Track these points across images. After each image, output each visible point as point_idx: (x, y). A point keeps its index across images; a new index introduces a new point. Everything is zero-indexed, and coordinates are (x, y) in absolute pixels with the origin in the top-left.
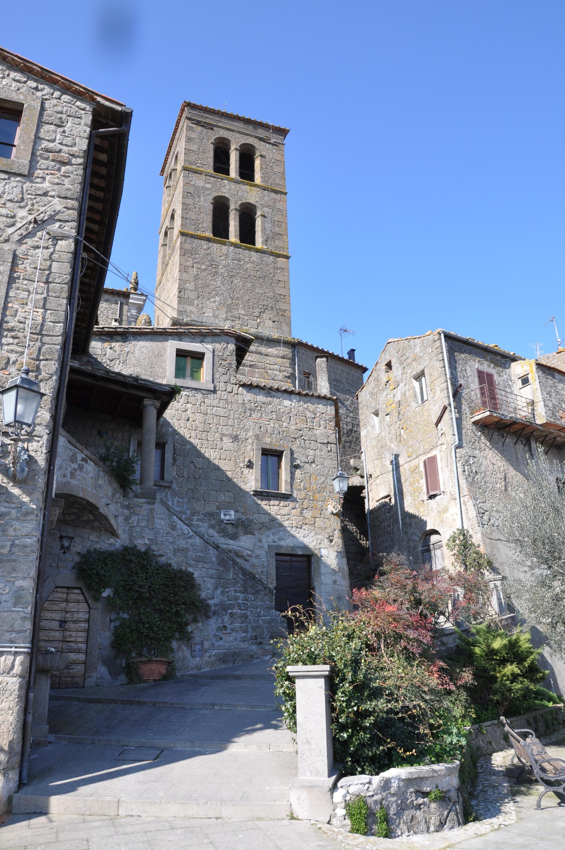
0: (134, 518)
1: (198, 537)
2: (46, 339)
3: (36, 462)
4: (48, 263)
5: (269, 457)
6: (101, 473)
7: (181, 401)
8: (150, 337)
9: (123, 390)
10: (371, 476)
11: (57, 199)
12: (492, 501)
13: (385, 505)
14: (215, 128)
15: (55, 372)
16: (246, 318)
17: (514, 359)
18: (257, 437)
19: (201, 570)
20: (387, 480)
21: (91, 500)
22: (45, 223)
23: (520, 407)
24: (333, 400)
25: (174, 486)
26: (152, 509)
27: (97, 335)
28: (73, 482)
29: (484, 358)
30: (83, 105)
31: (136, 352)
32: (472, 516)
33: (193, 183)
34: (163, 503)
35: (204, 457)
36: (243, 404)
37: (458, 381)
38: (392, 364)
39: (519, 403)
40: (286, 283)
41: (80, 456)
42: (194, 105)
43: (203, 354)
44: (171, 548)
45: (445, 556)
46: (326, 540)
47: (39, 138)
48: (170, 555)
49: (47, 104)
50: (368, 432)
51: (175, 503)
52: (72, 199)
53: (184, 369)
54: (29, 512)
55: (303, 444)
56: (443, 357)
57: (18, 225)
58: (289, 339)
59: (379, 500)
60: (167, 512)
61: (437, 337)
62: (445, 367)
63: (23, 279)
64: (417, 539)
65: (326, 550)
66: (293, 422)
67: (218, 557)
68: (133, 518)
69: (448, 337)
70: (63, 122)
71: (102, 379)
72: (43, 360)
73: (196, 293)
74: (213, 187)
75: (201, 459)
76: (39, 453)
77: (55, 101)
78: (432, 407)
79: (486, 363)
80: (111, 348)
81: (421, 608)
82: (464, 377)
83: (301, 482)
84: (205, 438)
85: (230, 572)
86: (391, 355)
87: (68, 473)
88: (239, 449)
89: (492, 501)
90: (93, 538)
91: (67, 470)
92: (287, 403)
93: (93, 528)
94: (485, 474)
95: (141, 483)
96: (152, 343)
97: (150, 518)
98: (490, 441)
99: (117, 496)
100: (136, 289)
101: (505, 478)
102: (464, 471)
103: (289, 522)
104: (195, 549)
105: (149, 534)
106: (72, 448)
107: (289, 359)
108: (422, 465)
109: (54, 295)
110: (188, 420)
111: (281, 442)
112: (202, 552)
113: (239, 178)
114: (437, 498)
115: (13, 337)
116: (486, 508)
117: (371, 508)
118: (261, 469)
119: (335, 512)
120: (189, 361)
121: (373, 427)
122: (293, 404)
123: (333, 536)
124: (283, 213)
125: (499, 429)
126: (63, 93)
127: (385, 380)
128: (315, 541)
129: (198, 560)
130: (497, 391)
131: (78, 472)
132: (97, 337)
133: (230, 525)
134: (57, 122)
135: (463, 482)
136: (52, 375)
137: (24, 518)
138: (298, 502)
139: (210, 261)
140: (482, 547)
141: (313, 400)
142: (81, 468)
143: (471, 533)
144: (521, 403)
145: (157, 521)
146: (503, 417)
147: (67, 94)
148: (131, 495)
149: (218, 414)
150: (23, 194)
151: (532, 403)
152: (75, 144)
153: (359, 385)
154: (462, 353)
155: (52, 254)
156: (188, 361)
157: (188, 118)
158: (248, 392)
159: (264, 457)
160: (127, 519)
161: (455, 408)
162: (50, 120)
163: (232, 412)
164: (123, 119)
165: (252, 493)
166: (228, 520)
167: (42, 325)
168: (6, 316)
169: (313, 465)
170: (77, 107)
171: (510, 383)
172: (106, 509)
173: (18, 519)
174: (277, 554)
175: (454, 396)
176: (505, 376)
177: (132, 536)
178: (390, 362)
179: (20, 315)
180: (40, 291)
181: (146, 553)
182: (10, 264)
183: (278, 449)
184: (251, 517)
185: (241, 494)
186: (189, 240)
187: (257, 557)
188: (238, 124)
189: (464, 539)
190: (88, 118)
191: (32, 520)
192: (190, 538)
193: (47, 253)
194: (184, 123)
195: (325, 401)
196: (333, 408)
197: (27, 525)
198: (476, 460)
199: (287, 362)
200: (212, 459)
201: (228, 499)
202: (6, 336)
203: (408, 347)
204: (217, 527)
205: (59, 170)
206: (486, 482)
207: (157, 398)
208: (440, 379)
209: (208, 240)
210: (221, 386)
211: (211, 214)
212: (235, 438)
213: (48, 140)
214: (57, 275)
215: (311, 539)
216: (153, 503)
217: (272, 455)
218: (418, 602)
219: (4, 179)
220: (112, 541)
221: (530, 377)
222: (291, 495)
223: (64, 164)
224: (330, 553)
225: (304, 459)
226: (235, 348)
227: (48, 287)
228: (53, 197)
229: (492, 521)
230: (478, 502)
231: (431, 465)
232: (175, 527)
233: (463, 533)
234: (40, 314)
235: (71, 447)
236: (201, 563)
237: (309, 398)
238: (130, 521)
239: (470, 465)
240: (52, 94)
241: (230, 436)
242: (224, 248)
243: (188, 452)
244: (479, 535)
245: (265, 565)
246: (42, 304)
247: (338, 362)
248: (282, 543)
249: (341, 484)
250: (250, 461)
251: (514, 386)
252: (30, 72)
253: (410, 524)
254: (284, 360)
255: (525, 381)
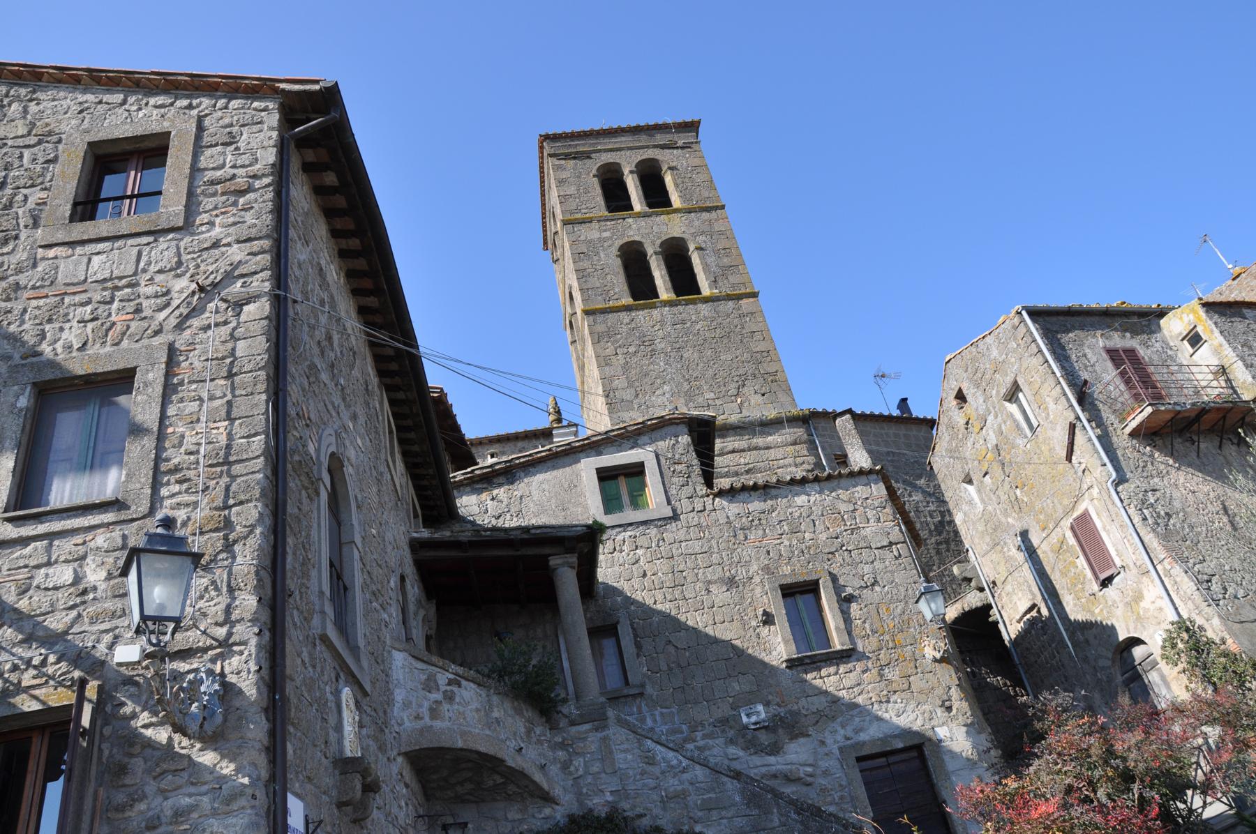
0: (578, 762)
1: (698, 767)
2: (237, 469)
3: (240, 691)
4: (230, 346)
5: (798, 597)
6: (495, 699)
7: (625, 548)
8: (549, 464)
9: (511, 553)
10: (994, 583)
11: (236, 246)
12: (1216, 555)
13: (1032, 623)
14: (593, 155)
15: (258, 520)
16: (718, 402)
17: (1161, 313)
18: (767, 569)
19: (719, 825)
20: (1021, 580)
21: (482, 749)
22: (219, 287)
23: (1204, 383)
24: (878, 472)
25: (649, 690)
26: (605, 739)
27: (467, 485)
28: (438, 724)
29: (1109, 327)
30: (263, 105)
31: (534, 493)
32: (1189, 592)
33: (582, 238)
34: (622, 723)
35: (688, 629)
36: (729, 523)
37: (1079, 376)
38: (965, 392)
39: (1199, 377)
40: (765, 334)
41: (442, 678)
42: (555, 135)
43: (641, 465)
44: (655, 797)
45: (1169, 679)
46: (939, 711)
47: (199, 170)
48: (657, 811)
49: (207, 122)
50: (965, 514)
51: (658, 718)
52: (260, 238)
53: (618, 498)
54: (240, 792)
55: (848, 559)
56: (1038, 346)
57: (175, 303)
58: (794, 412)
59: (1021, 619)
60: (632, 736)
61: (1016, 320)
62: (1047, 361)
63: (189, 382)
64: (1104, 664)
65: (945, 728)
66: (820, 527)
67: (743, 792)
68: (576, 763)
69: (1035, 314)
70: (234, 137)
71: (472, 544)
72: (235, 505)
73: (633, 390)
74: (613, 234)
75: (683, 633)
76: (244, 674)
77: (220, 114)
78: (1050, 433)
79: (1116, 335)
80: (493, 499)
81: (1136, 787)
82: (1086, 367)
83: (864, 622)
84: (681, 597)
85: (772, 813)
86: (959, 379)
87: (424, 711)
88: (742, 598)
89: (1216, 555)
90: (513, 814)
91: (420, 706)
92: (801, 500)
93: (509, 798)
94: (1185, 513)
95: (578, 697)
96: (555, 473)
97: (606, 753)
98: (1172, 455)
99: (538, 730)
100: (559, 420)
101: (1225, 509)
102: (1145, 519)
103: (865, 696)
104: (698, 789)
105: (612, 784)
106: (423, 666)
107: (805, 443)
108: (1069, 534)
109: (244, 392)
110: (645, 575)
111: (810, 566)
112: (712, 790)
113: (647, 209)
114: (1116, 580)
115: (180, 482)
116: (1210, 571)
117: (1013, 636)
118: (789, 621)
119: (938, 656)
120: (623, 483)
121: (970, 503)
122: (812, 499)
123: (950, 700)
124: (727, 235)
125: (1181, 432)
126: (230, 99)
127: (962, 421)
128: (920, 717)
129: (707, 807)
130: (1151, 369)
131: (446, 706)
132: (468, 489)
133: (763, 731)
134: (226, 139)
135: (1149, 538)
136: (253, 526)
137: (226, 808)
138: (868, 658)
139: (640, 338)
140: (1230, 641)
141: (844, 482)
142: (450, 697)
143: (1199, 621)
144: (1203, 377)
145: (619, 756)
146: (1178, 408)
147: (236, 98)
148: (563, 723)
149: (691, 551)
150: (179, 255)
151: (1223, 370)
152: (257, 160)
153: (928, 446)
154: (1068, 331)
155: (234, 329)
156: (620, 483)
157: (550, 155)
158: (731, 501)
159: (789, 600)
160: (565, 766)
161: (1089, 421)
162: (213, 140)
163: (713, 542)
164: (329, 99)
165: (784, 665)
166: (755, 724)
167: (229, 447)
168: (166, 449)
169: (877, 588)
170: (255, 109)
171: (1170, 352)
172: (519, 759)
173: (215, 813)
174: (859, 759)
175: (1081, 401)
176: (1157, 345)
177: (581, 794)
178: (960, 390)
179: (189, 443)
180: (219, 394)
181: (610, 818)
182: (163, 366)
183: (808, 578)
184: (796, 707)
185: (767, 672)
186: (600, 318)
187: (826, 773)
188: (623, 139)
189: (1190, 637)
190: (274, 119)
191: (243, 808)
192: (684, 770)
193: (224, 331)
194: (550, 163)
195: (864, 479)
196: (882, 486)
197: (234, 820)
198: (1158, 494)
199: (803, 449)
200: (701, 626)
201: (747, 688)
202: (168, 483)
203: (979, 356)
204: (741, 740)
205: (235, 204)
206: (1192, 527)
207: (570, 551)
208: (1046, 385)
209: (628, 308)
210: (685, 505)
211: (621, 271)
212: (731, 583)
213: (213, 169)
214: (246, 360)
215: (912, 717)
216: (605, 727)
217: (800, 593)
218: (1127, 777)
219: (148, 244)
220: (547, 811)
221: (1200, 329)
222: (853, 650)
223: (242, 193)
224: (954, 730)
225: (858, 583)
226: (689, 439)
227: (233, 383)
228: (229, 245)
229: (1231, 590)
230: (1190, 565)
231: (1084, 529)
232: (653, 758)
233: (1183, 626)
234: (221, 430)
235: (420, 665)
236: (715, 812)
237: (835, 482)
238: (572, 768)
239: (1152, 505)
240: (215, 106)
241: (721, 581)
242: (655, 312)
243: (661, 629)
244: (1216, 621)
245: (844, 783)
246: (223, 413)
247: (885, 425)
248: (863, 737)
249: (933, 605)
250: (765, 613)
251: (1179, 355)
252: (177, 89)
253: (1087, 641)
254: (797, 447)
255: (1195, 340)
